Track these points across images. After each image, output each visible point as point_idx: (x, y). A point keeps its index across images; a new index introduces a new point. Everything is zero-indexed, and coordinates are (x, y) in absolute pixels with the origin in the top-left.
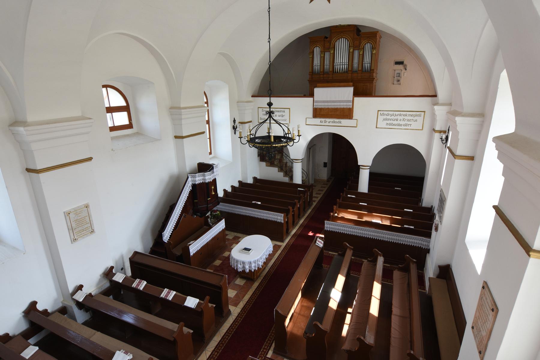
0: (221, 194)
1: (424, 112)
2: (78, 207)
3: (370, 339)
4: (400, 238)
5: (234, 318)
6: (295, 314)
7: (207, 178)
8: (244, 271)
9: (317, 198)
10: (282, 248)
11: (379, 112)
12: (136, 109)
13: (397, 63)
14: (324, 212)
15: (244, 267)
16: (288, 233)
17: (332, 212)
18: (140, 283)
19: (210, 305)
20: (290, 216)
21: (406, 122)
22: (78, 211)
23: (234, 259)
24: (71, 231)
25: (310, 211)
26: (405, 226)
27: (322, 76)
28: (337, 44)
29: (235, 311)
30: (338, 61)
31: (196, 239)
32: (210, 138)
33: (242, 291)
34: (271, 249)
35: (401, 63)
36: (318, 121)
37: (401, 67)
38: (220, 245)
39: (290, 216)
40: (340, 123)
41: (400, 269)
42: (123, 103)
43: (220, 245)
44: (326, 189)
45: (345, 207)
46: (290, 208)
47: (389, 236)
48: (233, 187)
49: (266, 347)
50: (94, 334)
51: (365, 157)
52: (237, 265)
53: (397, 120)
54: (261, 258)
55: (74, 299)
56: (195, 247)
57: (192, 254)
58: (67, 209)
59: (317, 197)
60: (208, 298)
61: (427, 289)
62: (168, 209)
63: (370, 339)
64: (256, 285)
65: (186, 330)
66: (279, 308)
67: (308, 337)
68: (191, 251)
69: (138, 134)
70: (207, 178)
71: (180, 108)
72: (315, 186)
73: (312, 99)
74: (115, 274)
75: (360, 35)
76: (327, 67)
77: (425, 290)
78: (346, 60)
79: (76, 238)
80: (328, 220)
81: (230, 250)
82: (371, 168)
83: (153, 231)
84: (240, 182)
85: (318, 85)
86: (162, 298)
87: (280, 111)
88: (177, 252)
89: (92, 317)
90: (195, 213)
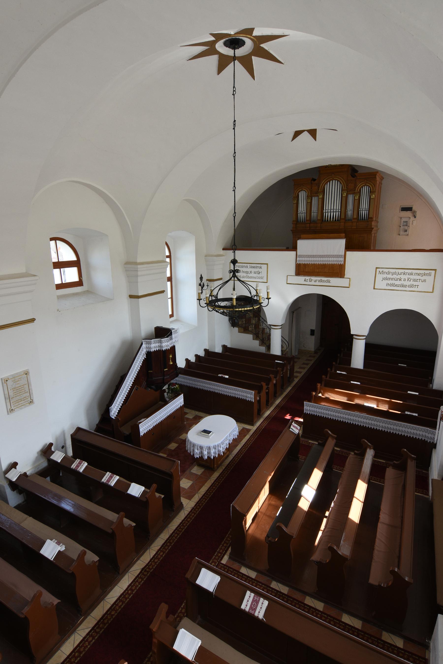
0: (181, 363)
1: (435, 270)
2: (17, 373)
3: (345, 549)
4: (398, 428)
5: (187, 513)
6: (259, 513)
7: (164, 344)
8: (201, 458)
9: (300, 372)
10: (251, 433)
11: (378, 270)
12: (88, 265)
13: (404, 209)
14: (307, 390)
15: (201, 453)
16: (260, 414)
17: (316, 391)
18: (80, 463)
19: (157, 495)
20: (263, 394)
21: (412, 283)
22: (16, 378)
23: (191, 443)
24: (8, 401)
25: (290, 388)
26: (406, 413)
27: (308, 225)
28: (327, 187)
29: (188, 504)
30: (328, 207)
31: (147, 417)
32: (172, 298)
33: (199, 481)
34: (236, 433)
35: (409, 209)
36: (301, 279)
37: (409, 213)
38: (176, 426)
39: (263, 394)
40: (329, 282)
41: (395, 467)
42: (73, 258)
43: (176, 426)
44: (312, 362)
45: (332, 386)
46: (264, 384)
47: (384, 425)
48: (197, 356)
49: (221, 551)
50: (27, 518)
51: (360, 325)
52: (193, 450)
53: (400, 280)
54: (222, 443)
55: (7, 478)
56: (146, 426)
57: (142, 434)
58: (5, 375)
59: (300, 373)
60: (154, 486)
61: (430, 494)
62: (119, 378)
63: (345, 549)
64: (216, 475)
65: (127, 522)
66: (236, 504)
67: (270, 541)
68: (141, 430)
69: (88, 292)
70: (164, 344)
71: (136, 264)
72: (299, 358)
73: (294, 252)
74: (53, 452)
75: (355, 177)
76: (314, 214)
77: (428, 495)
78: (337, 206)
79: (13, 408)
80: (310, 401)
81: (187, 433)
82: (367, 338)
83: (100, 405)
84: (206, 350)
85: (302, 236)
86: (103, 483)
87: (256, 267)
88: (126, 430)
89: (25, 501)
90: (149, 385)
